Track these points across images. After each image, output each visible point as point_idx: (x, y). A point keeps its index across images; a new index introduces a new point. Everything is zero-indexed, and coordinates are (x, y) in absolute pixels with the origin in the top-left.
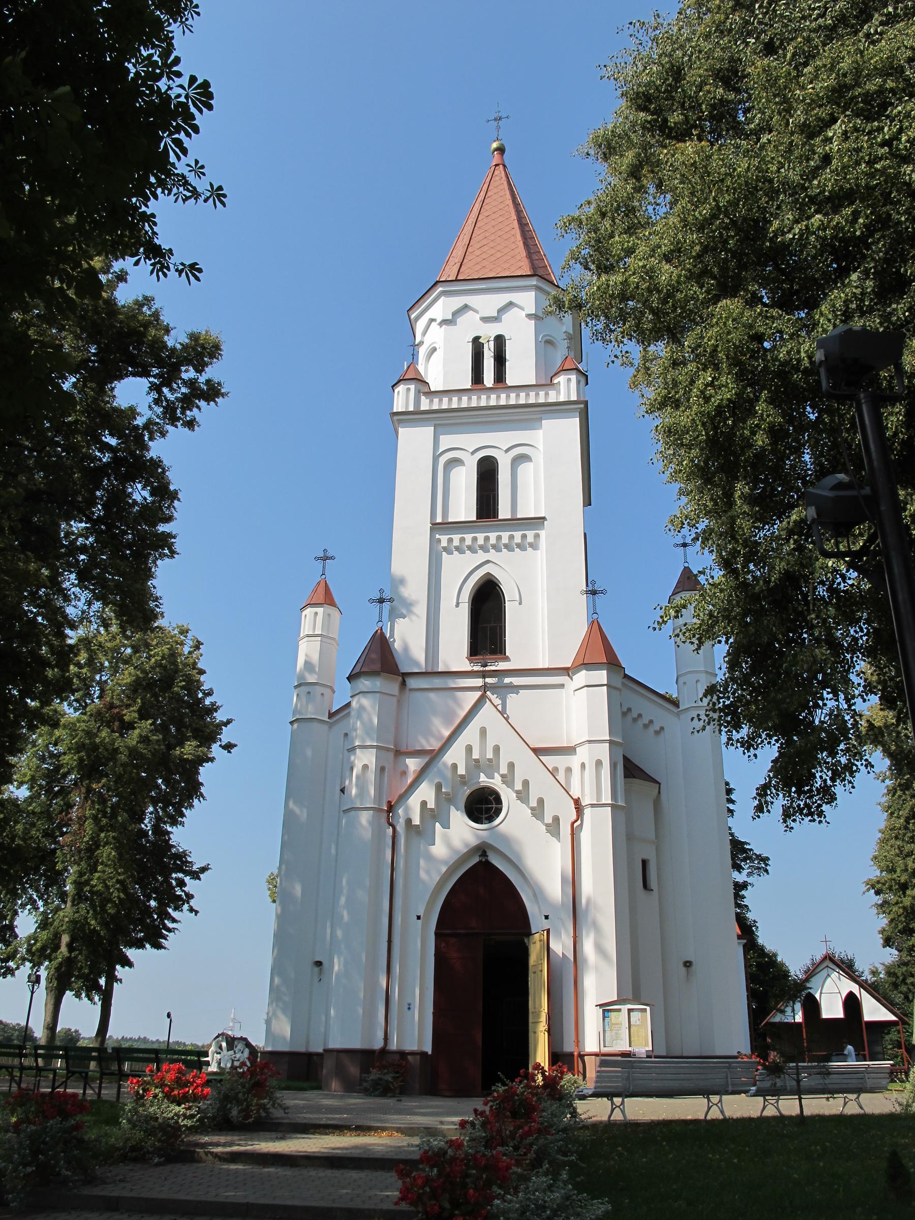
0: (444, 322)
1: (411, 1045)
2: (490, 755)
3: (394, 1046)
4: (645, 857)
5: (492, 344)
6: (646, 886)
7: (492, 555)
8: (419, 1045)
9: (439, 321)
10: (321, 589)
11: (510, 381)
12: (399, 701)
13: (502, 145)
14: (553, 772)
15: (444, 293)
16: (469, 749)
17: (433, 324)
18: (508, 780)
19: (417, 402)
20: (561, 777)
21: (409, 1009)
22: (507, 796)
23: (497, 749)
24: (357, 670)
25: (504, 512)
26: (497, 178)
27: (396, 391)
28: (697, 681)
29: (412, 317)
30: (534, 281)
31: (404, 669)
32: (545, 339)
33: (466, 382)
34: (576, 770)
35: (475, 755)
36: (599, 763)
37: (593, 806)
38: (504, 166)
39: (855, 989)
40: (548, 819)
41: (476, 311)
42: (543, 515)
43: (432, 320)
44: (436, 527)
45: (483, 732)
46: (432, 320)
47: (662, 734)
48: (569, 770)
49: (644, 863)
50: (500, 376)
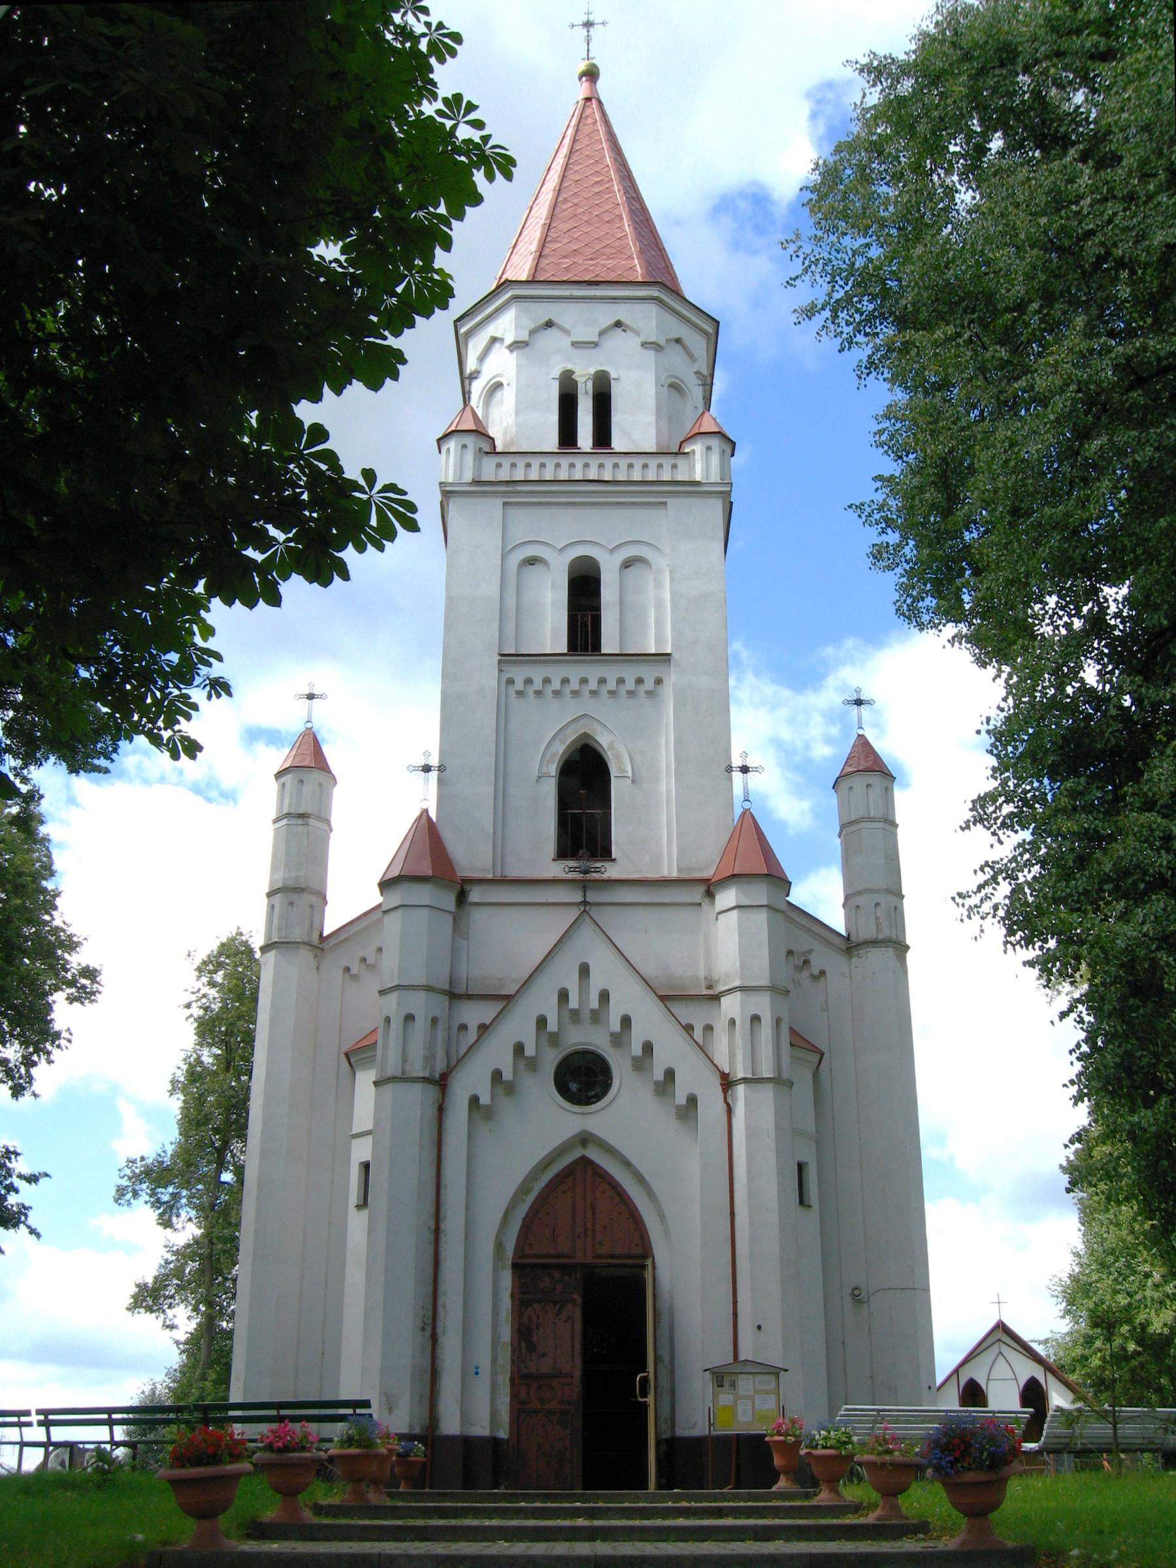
0: (516, 346)
1: (481, 1429)
2: (594, 1003)
3: (450, 1426)
4: (803, 1159)
5: (590, 385)
6: (802, 1201)
7: (588, 705)
8: (492, 1429)
9: (508, 342)
10: (309, 750)
11: (618, 444)
12: (454, 920)
13: (594, 66)
14: (689, 1029)
15: (516, 298)
16: (563, 996)
17: (497, 345)
18: (619, 1039)
19: (478, 466)
20: (698, 1034)
21: (477, 1373)
22: (619, 1065)
23: (604, 996)
24: (395, 873)
25: (609, 644)
26: (590, 121)
27: (444, 449)
28: (877, 904)
29: (462, 331)
30: (654, 292)
31: (463, 872)
32: (669, 381)
33: (551, 441)
34: (721, 1028)
35: (573, 1003)
36: (756, 1019)
37: (745, 1080)
38: (600, 102)
39: (1039, 1374)
40: (681, 1099)
41: (566, 331)
42: (669, 652)
43: (494, 340)
44: (507, 659)
45: (584, 971)
46: (494, 340)
47: (822, 979)
48: (709, 1028)
49: (801, 1167)
50: (602, 436)
